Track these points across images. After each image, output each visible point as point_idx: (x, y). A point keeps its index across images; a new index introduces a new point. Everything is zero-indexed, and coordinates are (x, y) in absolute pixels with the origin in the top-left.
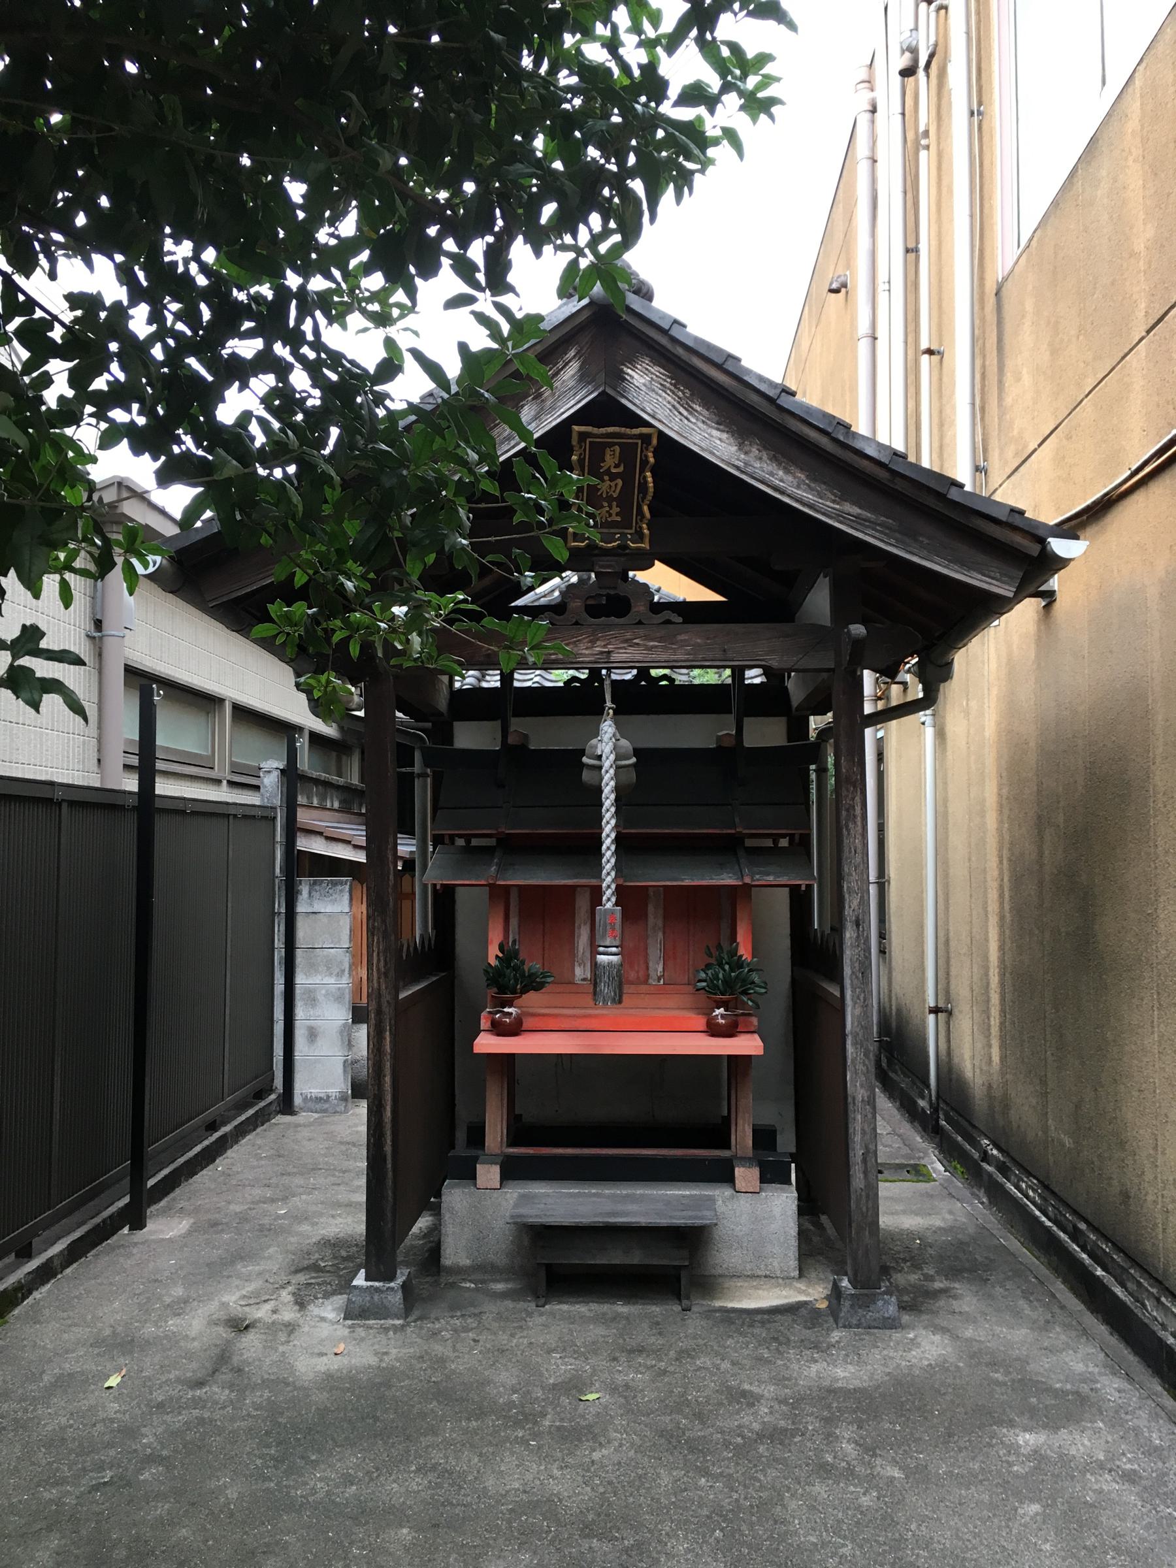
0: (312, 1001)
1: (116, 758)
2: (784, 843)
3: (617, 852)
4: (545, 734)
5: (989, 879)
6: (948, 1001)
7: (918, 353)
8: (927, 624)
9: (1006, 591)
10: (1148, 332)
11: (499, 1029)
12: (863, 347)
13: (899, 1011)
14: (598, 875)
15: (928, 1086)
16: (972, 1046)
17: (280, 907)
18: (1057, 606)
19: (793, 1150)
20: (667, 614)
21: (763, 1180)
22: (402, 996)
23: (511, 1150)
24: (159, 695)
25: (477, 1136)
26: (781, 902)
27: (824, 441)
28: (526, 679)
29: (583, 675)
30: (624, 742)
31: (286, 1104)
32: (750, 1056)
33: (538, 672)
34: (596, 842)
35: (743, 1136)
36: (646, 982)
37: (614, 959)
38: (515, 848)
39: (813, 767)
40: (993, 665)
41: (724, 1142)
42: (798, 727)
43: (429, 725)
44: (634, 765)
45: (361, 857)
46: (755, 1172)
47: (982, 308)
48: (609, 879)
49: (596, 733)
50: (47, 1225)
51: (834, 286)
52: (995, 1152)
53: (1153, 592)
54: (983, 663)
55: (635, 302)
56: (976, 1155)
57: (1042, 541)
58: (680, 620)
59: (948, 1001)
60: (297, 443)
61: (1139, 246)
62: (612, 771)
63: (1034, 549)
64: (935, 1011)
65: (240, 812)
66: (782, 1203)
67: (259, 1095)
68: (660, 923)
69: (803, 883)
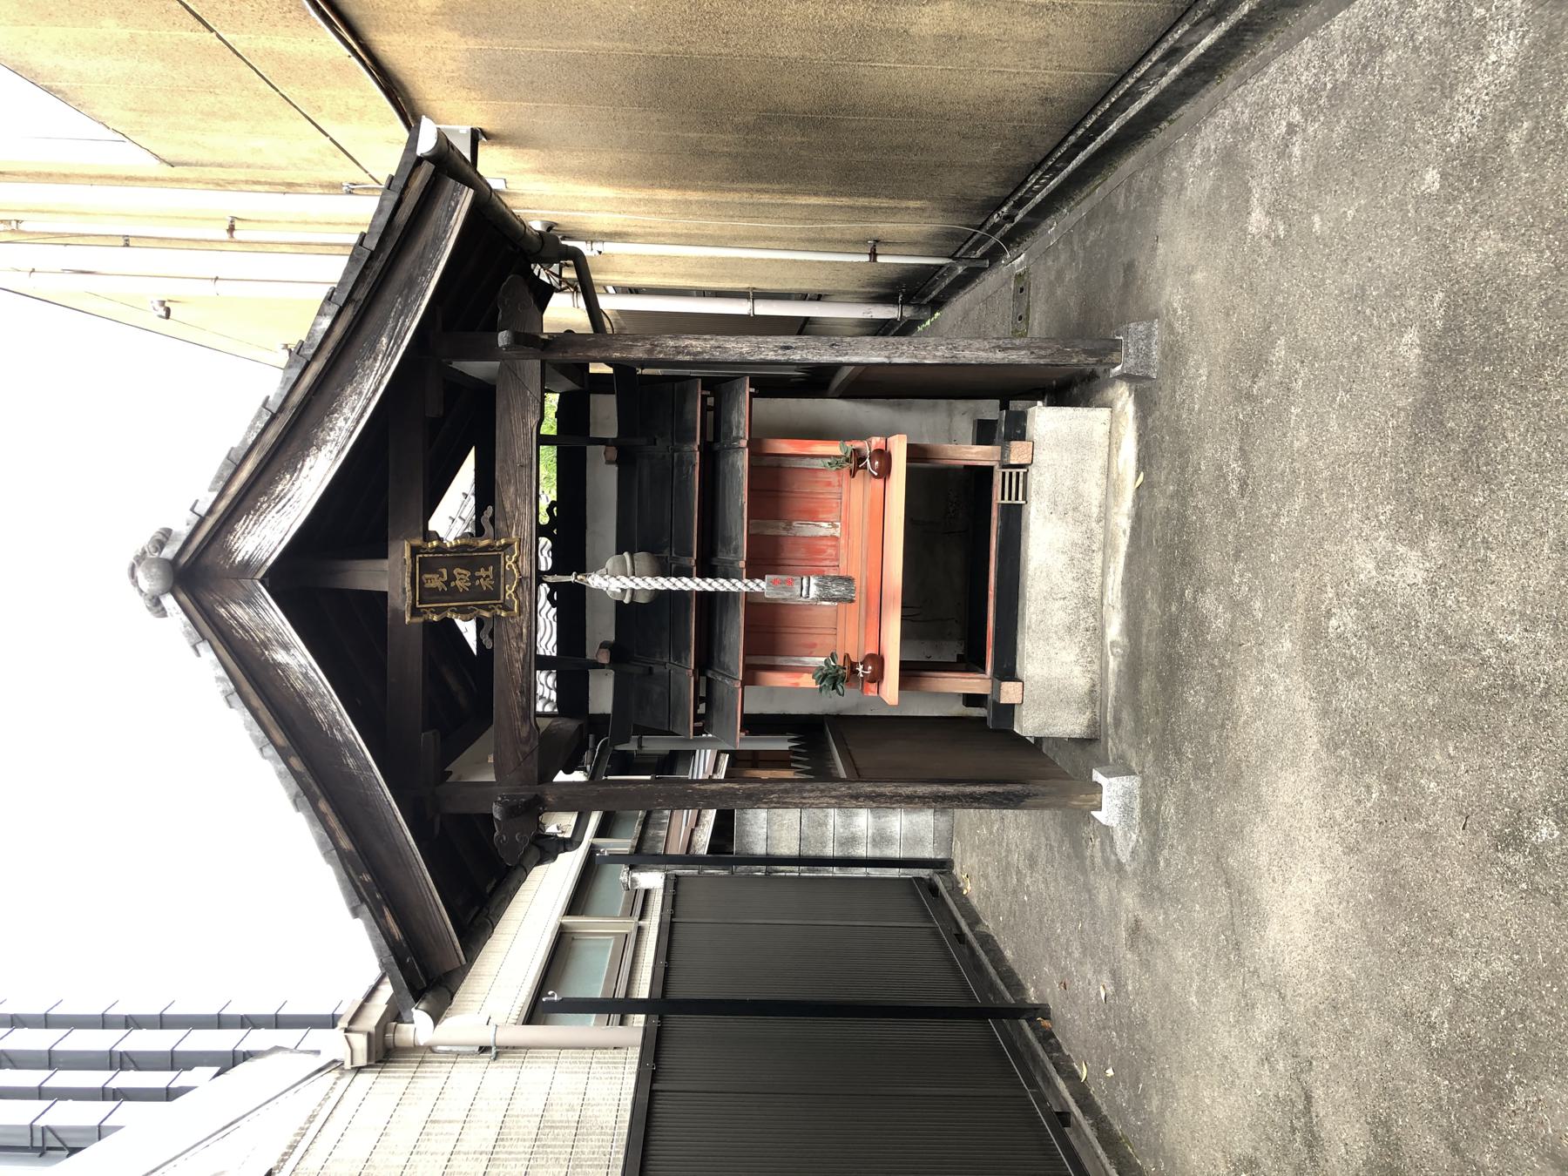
0: (852, 840)
1: (615, 1033)
3: (714, 576)
4: (601, 629)
6: (865, 242)
8: (505, 261)
9: (467, 196)
10: (212, 30)
11: (878, 677)
13: (873, 285)
14: (735, 595)
15: (941, 266)
16: (908, 235)
17: (760, 870)
18: (486, 128)
20: (485, 520)
21: (1022, 437)
22: (843, 775)
23: (989, 669)
25: (972, 700)
27: (316, 367)
28: (547, 643)
30: (609, 564)
31: (943, 865)
32: (901, 662)
34: (703, 595)
36: (836, 539)
37: (813, 581)
38: (708, 659)
41: (988, 471)
42: (601, 383)
43: (591, 737)
44: (632, 555)
45: (710, 816)
47: (187, 180)
48: (739, 584)
49: (600, 592)
50: (1042, 1100)
51: (164, 314)
52: (1005, 209)
53: (473, 44)
56: (1008, 226)
58: (490, 508)
59: (865, 242)
61: (124, 34)
62: (637, 580)
63: (427, 168)
64: (873, 255)
65: (668, 911)
66: (1044, 419)
67: (933, 889)
68: (782, 524)
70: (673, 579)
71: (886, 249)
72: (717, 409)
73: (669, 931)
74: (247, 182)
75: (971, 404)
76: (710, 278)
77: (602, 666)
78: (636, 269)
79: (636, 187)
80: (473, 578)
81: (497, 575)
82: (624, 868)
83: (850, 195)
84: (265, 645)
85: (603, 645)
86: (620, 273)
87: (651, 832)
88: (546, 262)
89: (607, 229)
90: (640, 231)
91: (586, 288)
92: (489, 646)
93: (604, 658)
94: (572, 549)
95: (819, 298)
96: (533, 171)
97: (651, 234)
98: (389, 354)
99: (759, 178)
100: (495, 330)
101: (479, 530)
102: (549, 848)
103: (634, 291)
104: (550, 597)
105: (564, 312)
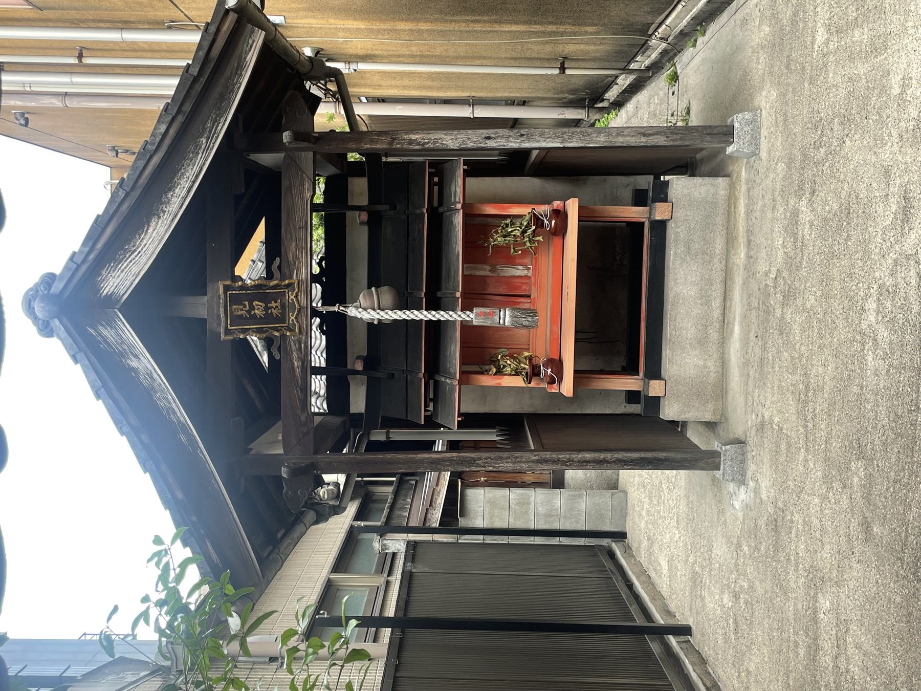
2: (436, 179)
4: (357, 345)
5: (467, 29)
7: (80, 64)
8: (286, 81)
12: (73, 103)
14: (454, 322)
19: (652, 177)
21: (665, 200)
23: (641, 374)
24: (323, 614)
25: (633, 397)
26: (479, 184)
27: (156, 160)
28: (319, 359)
29: (318, 320)
33: (313, 352)
34: (429, 322)
35: (635, 213)
38: (435, 366)
39: (384, 159)
40: (312, 21)
42: (356, 169)
46: (658, 205)
51: (23, 122)
54: (311, 28)
55: (57, 287)
57: (227, 11)
58: (278, 259)
60: (373, 438)
62: (382, 313)
63: (232, 17)
64: (563, 69)
66: (678, 185)
69: (462, 167)
70: (408, 312)
71: (573, 64)
72: (441, 185)
73: (408, 579)
74: (94, 21)
75: (632, 179)
76: (439, 89)
77: (357, 373)
78: (383, 83)
79: (381, 21)
80: (266, 308)
81: (283, 306)
82: (376, 537)
83: (541, 23)
84: (123, 355)
85: (358, 358)
86: (370, 86)
87: (397, 513)
88: (315, 79)
89: (360, 52)
90: (385, 53)
91: (344, 98)
92: (277, 357)
93: (359, 366)
94: (335, 283)
95: (524, 103)
96: (305, 10)
97: (393, 56)
98: (207, 149)
99: (473, 11)
100: (280, 131)
101: (270, 275)
102: (323, 513)
103: (382, 100)
104: (320, 326)
105: (328, 117)
